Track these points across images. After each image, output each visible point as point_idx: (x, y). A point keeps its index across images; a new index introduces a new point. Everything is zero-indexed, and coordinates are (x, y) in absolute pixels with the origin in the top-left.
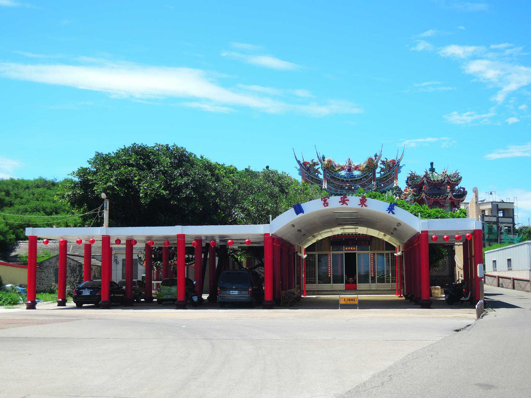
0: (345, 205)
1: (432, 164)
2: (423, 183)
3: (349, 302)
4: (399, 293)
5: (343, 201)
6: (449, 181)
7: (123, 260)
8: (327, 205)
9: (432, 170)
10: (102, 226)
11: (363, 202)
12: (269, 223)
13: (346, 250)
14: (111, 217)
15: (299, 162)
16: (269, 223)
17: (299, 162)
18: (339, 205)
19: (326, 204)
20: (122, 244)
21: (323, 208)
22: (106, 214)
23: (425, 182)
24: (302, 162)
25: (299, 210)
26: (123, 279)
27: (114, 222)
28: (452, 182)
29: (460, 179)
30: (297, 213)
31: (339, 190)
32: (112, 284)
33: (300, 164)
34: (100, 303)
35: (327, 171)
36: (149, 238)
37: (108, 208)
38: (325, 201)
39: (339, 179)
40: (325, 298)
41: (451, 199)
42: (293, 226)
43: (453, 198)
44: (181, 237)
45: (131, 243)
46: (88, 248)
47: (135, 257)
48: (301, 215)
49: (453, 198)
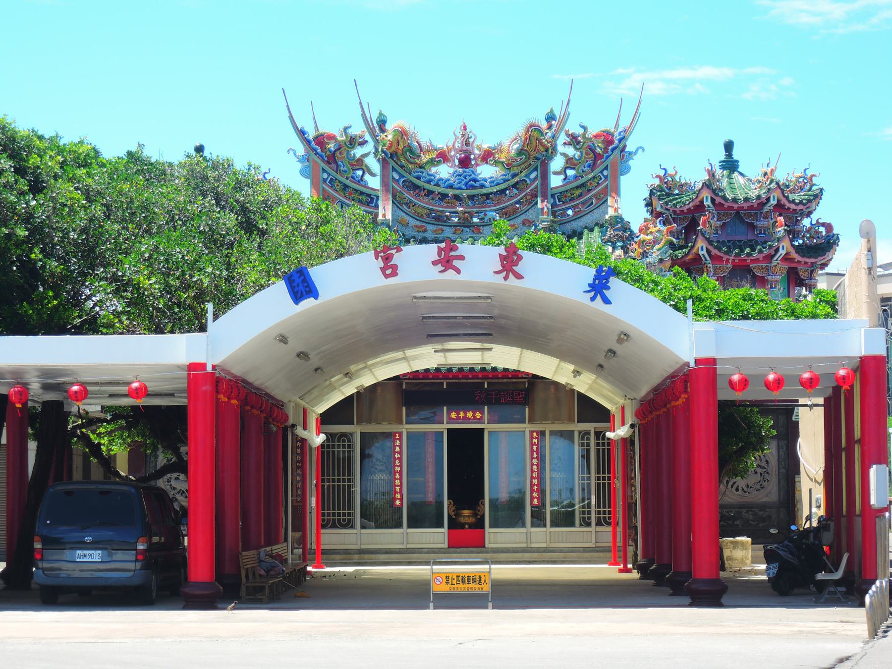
0: (450, 274)
1: (729, 147)
5: (446, 262)
6: (784, 201)
8: (394, 274)
9: (730, 165)
13: (450, 421)
15: (301, 133)
17: (301, 133)
18: (434, 273)
23: (707, 203)
24: (311, 134)
28: (793, 206)
31: (430, 227)
35: (392, 163)
41: (786, 258)
42: (283, 339)
43: (794, 255)
48: (308, 303)
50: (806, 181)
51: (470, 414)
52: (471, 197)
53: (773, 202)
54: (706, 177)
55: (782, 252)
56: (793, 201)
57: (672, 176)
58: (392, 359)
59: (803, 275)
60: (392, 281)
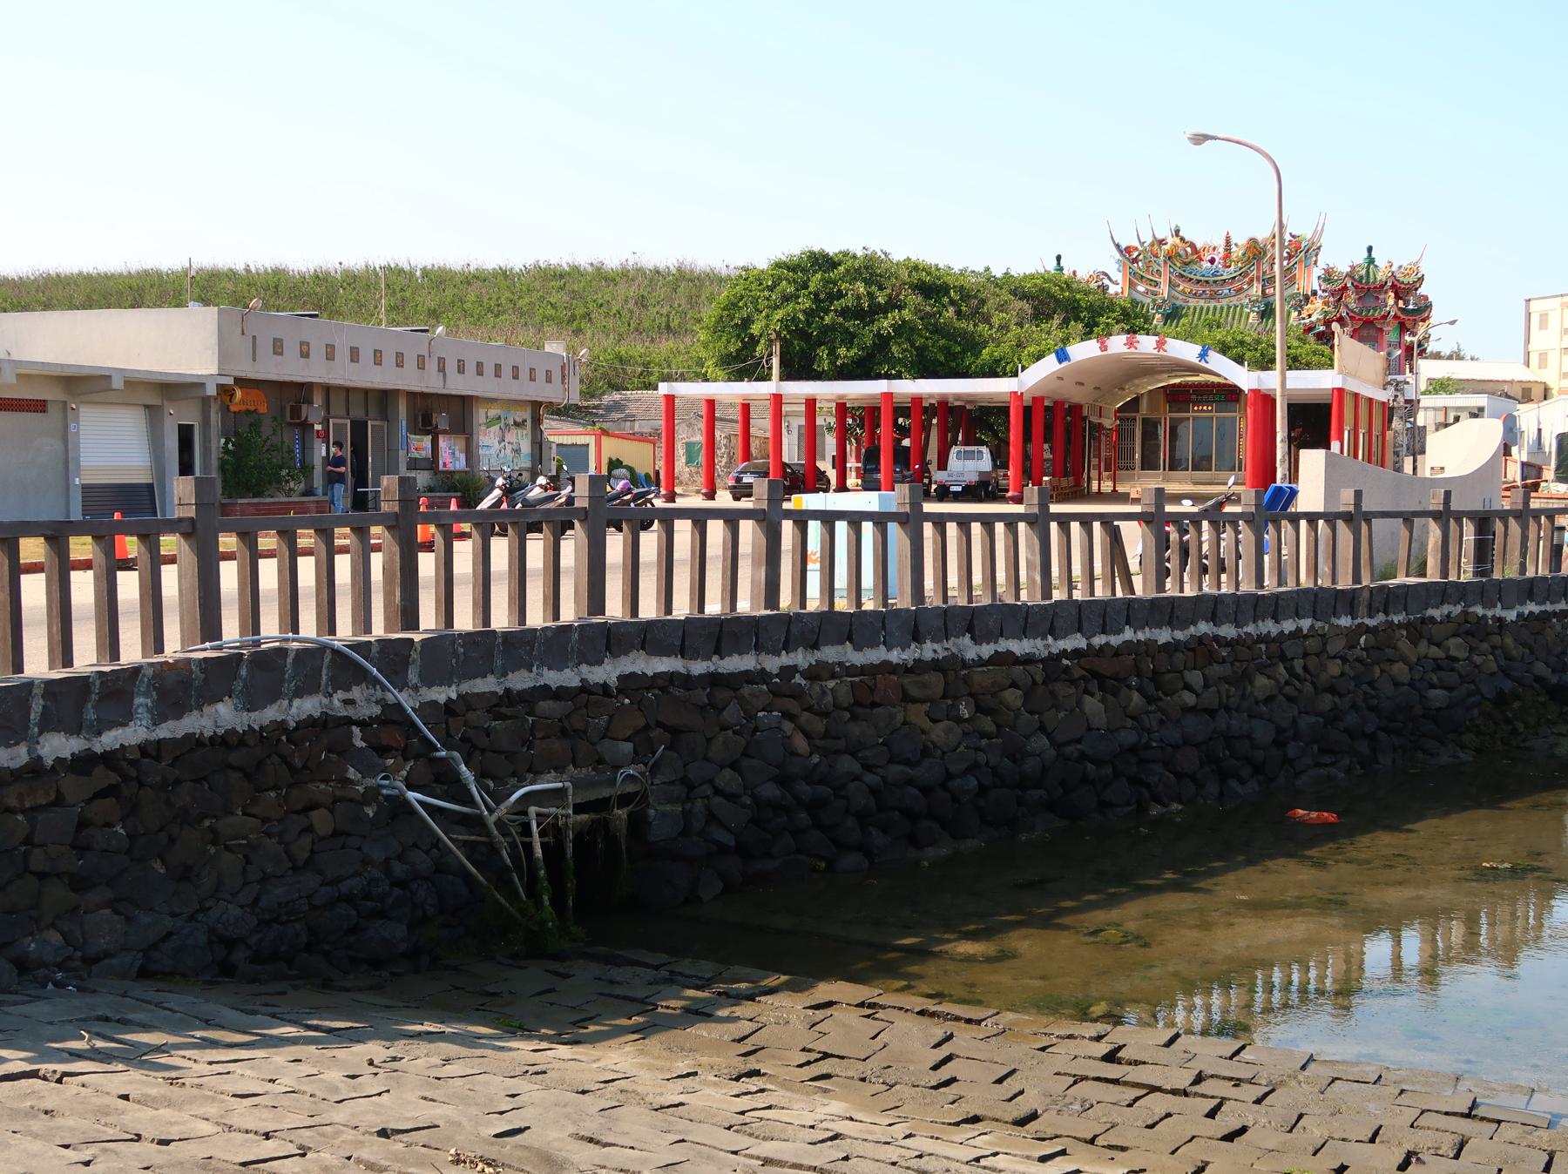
0: (1133, 350)
1: (1370, 249)
2: (1345, 288)
5: (1130, 344)
6: (1396, 283)
8: (1106, 350)
9: (1371, 261)
10: (770, 380)
11: (1160, 345)
13: (1194, 411)
15: (1118, 246)
17: (1118, 246)
18: (1125, 349)
19: (1104, 348)
20: (1070, 1075)
21: (1099, 353)
23: (1349, 285)
24: (1123, 246)
25: (1062, 357)
26: (544, 621)
27: (789, 374)
28: (1403, 286)
29: (1421, 279)
30: (1060, 361)
31: (1191, 300)
32: (785, 465)
33: (1121, 251)
35: (1169, 263)
36: (841, 397)
37: (778, 353)
38: (1102, 343)
39: (1191, 279)
40: (803, 449)
41: (1395, 317)
42: (1060, 378)
43: (1399, 314)
45: (811, 403)
46: (746, 408)
48: (1065, 364)
49: (1399, 314)
50: (1414, 268)
51: (1205, 408)
52: (1215, 282)
53: (1389, 284)
54: (1349, 269)
55: (1392, 314)
56: (1403, 283)
57: (1332, 268)
58: (58, 637)
59: (1408, 326)
60: (1104, 353)
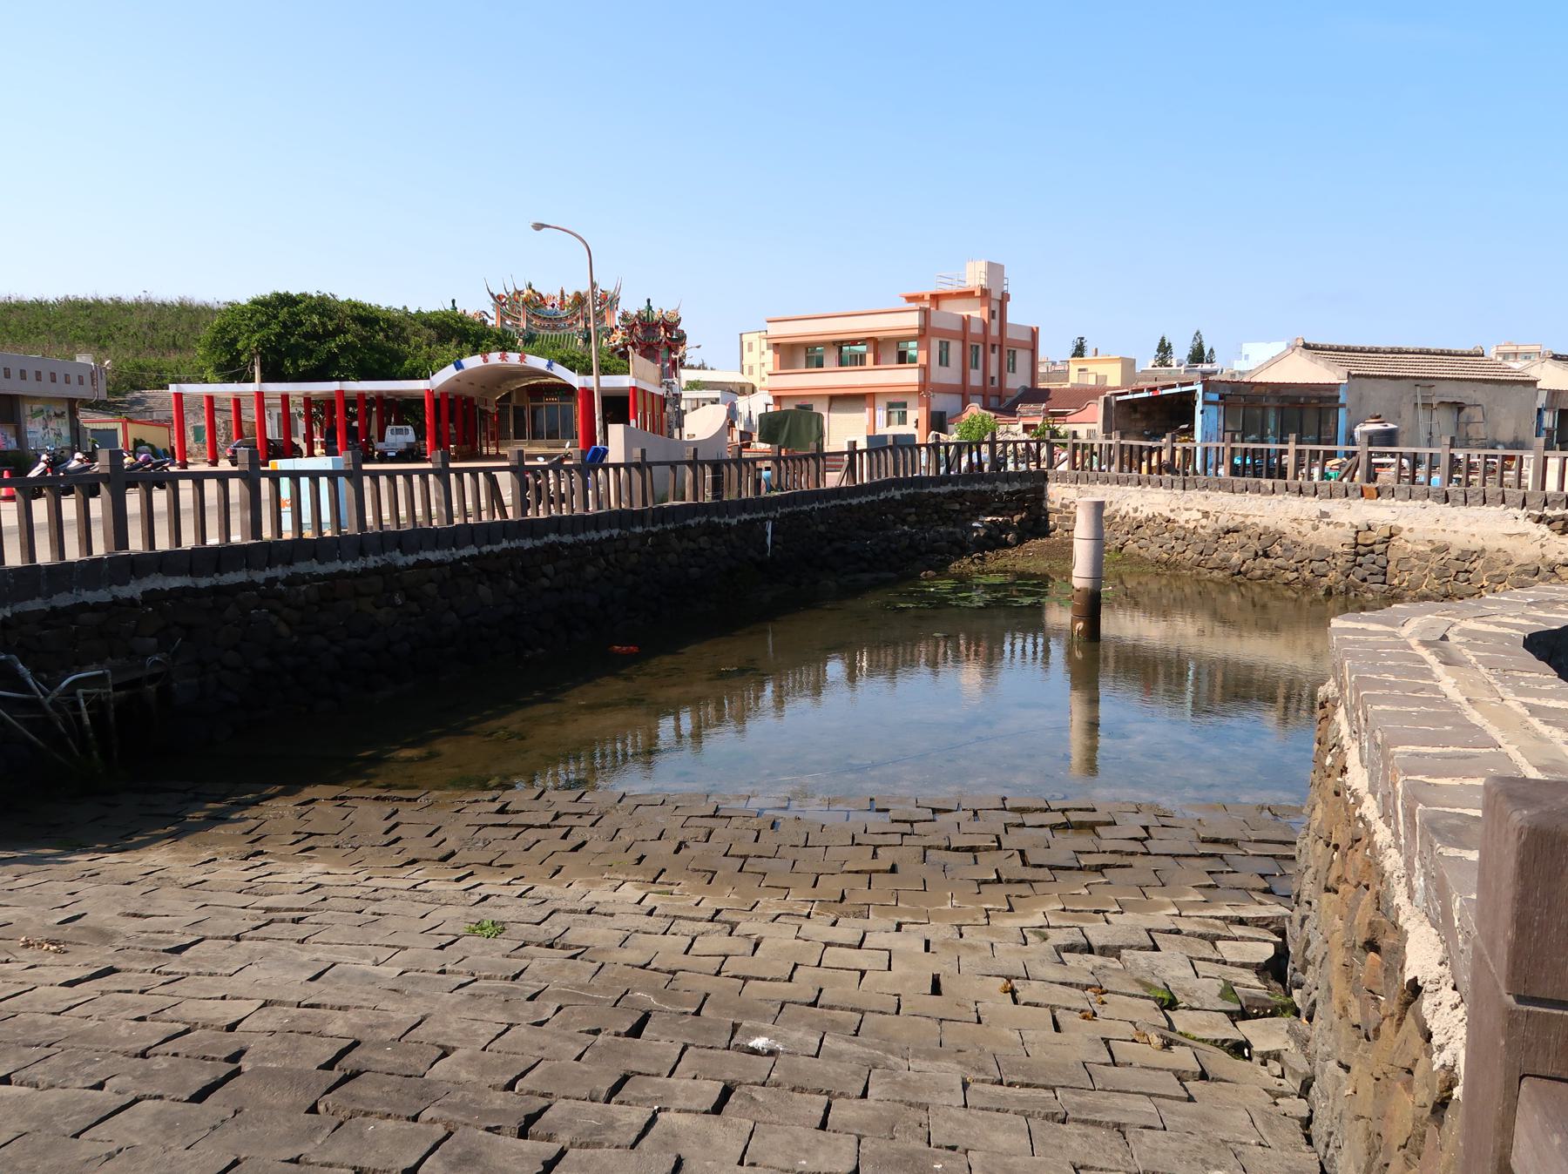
1: (649, 301)
3: (837, 457)
4: (207, 452)
5: (503, 358)
7: (278, 414)
12: (428, 378)
14: (262, 370)
15: (492, 295)
16: (428, 378)
17: (492, 295)
22: (257, 370)
24: (496, 295)
25: (459, 366)
26: (81, 556)
27: (266, 378)
30: (457, 369)
32: (269, 441)
34: (617, 647)
44: (341, 393)
45: (285, 398)
47: (292, 410)
48: (460, 371)
